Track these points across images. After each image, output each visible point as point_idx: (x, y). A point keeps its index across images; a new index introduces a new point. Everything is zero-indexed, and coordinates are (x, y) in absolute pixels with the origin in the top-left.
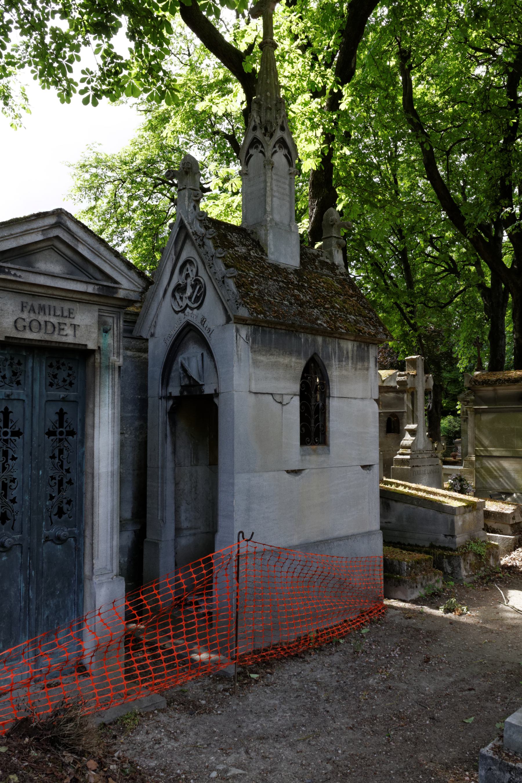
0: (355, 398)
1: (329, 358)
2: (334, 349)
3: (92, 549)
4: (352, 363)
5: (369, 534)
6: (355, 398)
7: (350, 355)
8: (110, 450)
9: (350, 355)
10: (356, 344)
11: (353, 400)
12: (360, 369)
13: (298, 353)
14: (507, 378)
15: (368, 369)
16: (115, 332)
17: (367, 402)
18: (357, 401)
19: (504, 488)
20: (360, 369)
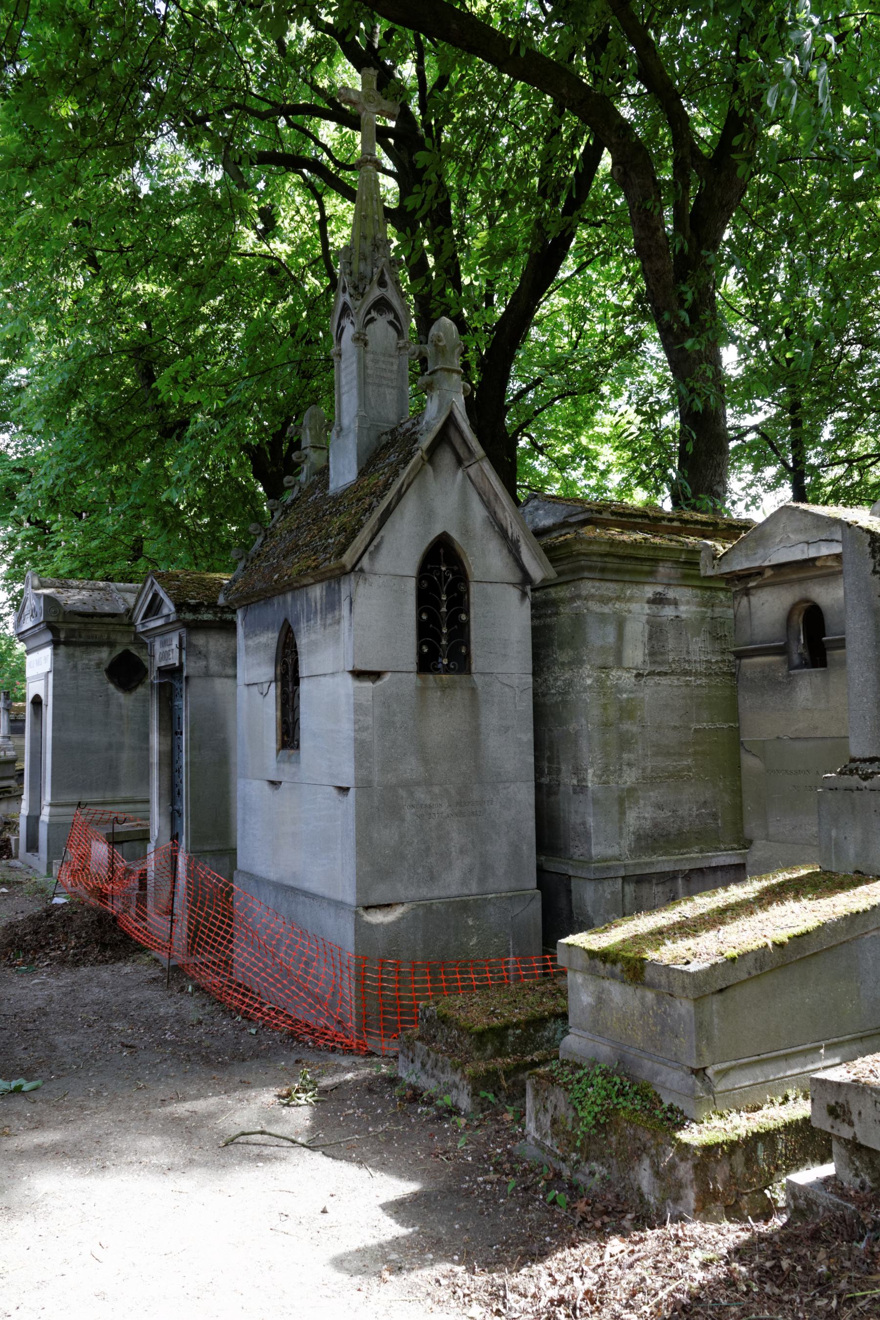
0: (325, 675)
1: (298, 622)
2: (302, 605)
3: (174, 887)
4: (321, 619)
5: (338, 905)
6: (325, 675)
7: (319, 607)
8: (749, 948)
9: (319, 607)
10: (324, 584)
11: (322, 678)
12: (330, 625)
13: (267, 628)
14: (643, 1075)
15: (338, 622)
16: (645, 923)
17: (339, 679)
18: (327, 678)
19: (464, 479)
20: (330, 625)
